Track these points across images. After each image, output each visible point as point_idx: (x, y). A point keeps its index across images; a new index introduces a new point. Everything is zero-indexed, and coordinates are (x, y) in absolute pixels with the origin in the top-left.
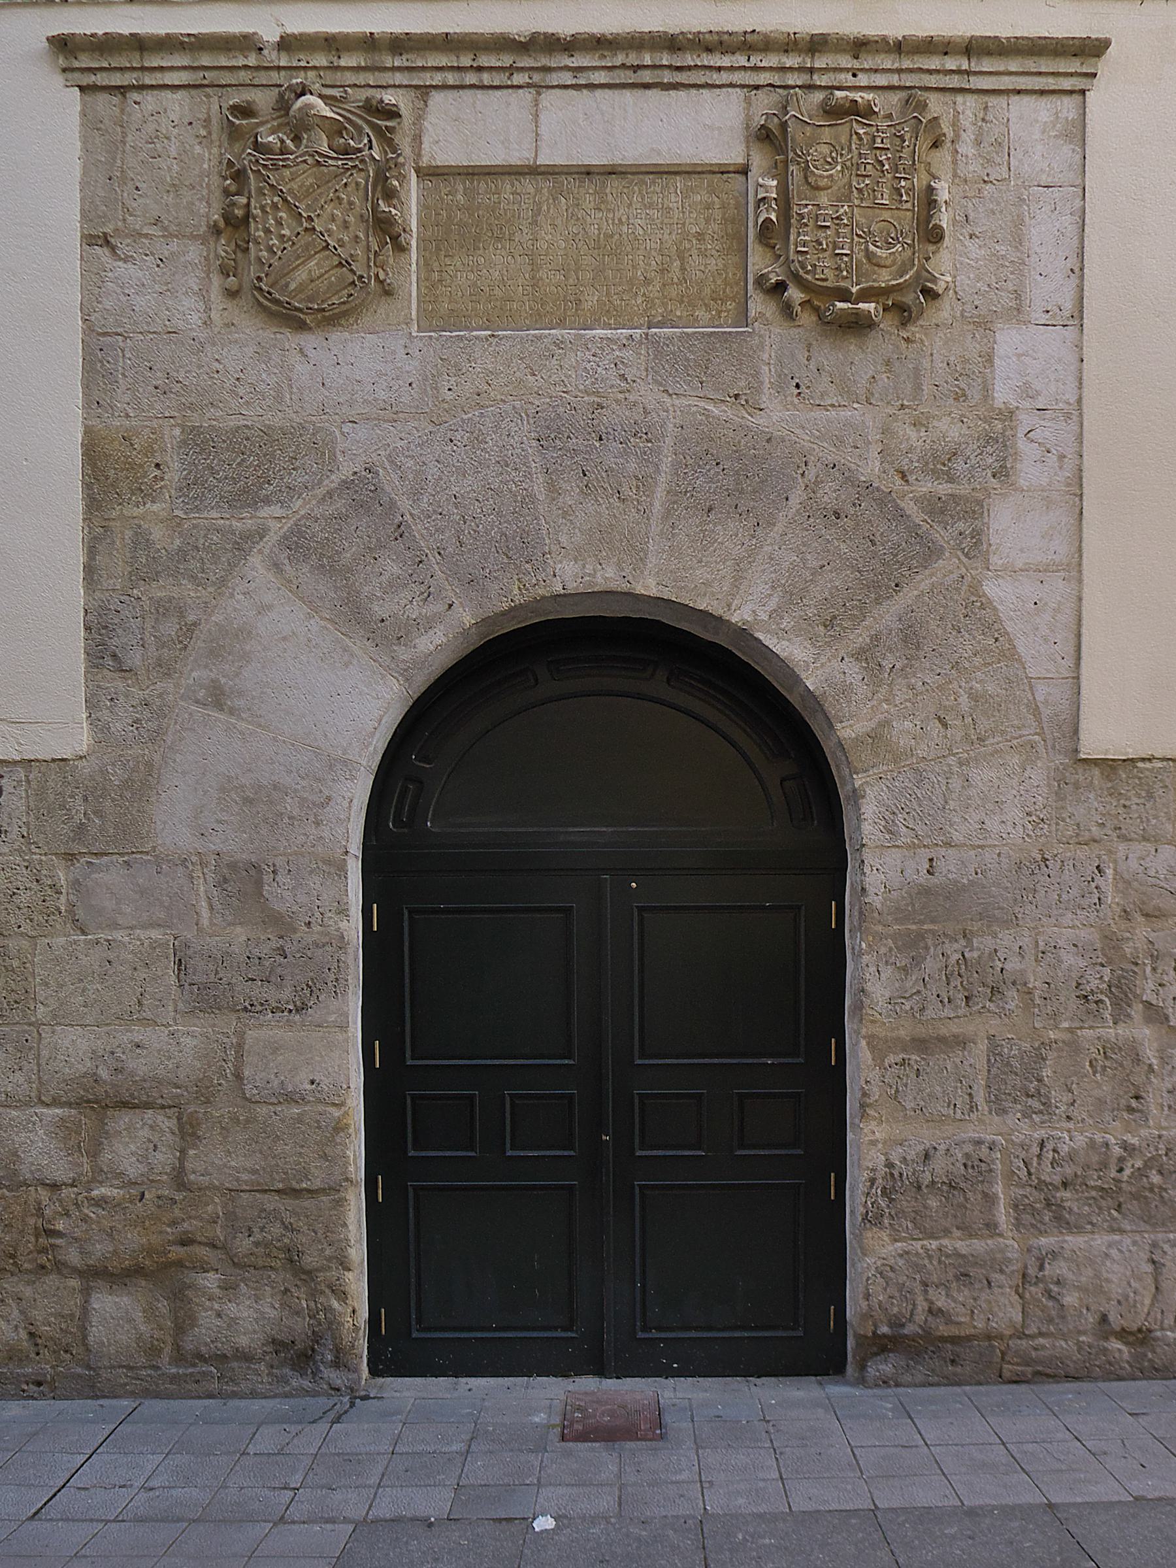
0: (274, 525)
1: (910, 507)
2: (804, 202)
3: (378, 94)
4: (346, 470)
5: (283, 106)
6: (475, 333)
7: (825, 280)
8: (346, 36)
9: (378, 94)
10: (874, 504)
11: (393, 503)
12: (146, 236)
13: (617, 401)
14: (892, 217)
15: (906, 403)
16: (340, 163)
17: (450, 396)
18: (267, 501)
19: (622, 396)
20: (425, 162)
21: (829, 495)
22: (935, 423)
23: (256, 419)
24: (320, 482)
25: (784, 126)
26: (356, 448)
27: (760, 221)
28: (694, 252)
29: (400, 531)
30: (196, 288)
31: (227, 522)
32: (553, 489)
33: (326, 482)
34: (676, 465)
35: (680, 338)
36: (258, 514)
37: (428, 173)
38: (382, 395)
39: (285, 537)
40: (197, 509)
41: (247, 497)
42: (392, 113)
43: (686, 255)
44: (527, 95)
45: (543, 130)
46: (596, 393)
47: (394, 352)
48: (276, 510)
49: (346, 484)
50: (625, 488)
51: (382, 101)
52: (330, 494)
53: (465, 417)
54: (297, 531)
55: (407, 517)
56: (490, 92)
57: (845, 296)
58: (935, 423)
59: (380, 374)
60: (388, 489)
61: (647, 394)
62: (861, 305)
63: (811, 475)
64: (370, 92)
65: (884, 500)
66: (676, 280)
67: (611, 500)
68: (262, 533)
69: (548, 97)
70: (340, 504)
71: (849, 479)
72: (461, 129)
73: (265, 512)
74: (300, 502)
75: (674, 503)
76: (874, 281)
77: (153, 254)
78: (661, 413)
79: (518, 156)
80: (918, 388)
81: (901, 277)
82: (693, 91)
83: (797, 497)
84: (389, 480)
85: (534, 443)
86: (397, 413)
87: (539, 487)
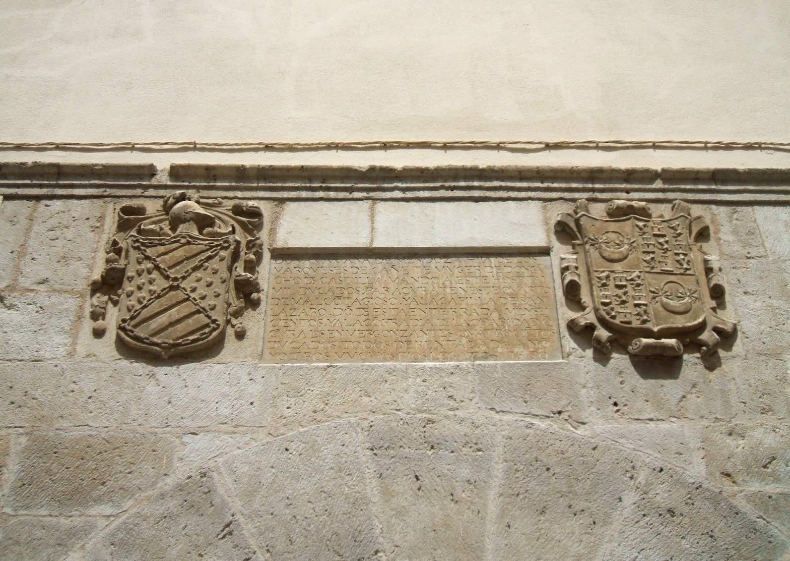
0: (102, 523)
1: (741, 504)
2: (602, 269)
3: (244, 203)
4: (180, 472)
5: (167, 208)
6: (314, 364)
7: (629, 323)
8: (330, 169)
9: (244, 203)
10: (707, 503)
11: (224, 504)
12: (32, 290)
13: (446, 417)
14: (678, 279)
15: (719, 416)
16: (207, 242)
17: (287, 413)
18: (98, 500)
19: (452, 413)
20: (279, 244)
21: (662, 495)
22: (751, 433)
23: (100, 429)
24: (154, 483)
25: (577, 221)
26: (195, 453)
27: (566, 281)
28: (510, 307)
29: (228, 530)
30: (67, 328)
31: (55, 520)
32: (387, 493)
33: (159, 485)
34: (507, 472)
35: (503, 366)
36: (87, 512)
37: (282, 254)
38: (226, 411)
39: (112, 535)
40: (28, 507)
41: (76, 496)
42: (256, 214)
43: (503, 309)
44: (366, 204)
45: (377, 225)
46: (428, 411)
47: (239, 379)
48: (108, 510)
49: (180, 488)
50: (459, 490)
51: (247, 205)
52: (162, 496)
53: (302, 430)
54: (126, 528)
55: (238, 517)
56: (335, 202)
57: (648, 334)
58: (751, 433)
59: (225, 395)
60: (221, 491)
61: (474, 410)
62: (663, 340)
63: (641, 477)
64: (237, 201)
65: (716, 499)
66: (495, 326)
67: (445, 502)
68: (87, 530)
69: (380, 206)
70: (172, 504)
71: (678, 482)
72: (302, 223)
73: (95, 510)
74: (131, 502)
75: (508, 503)
76: (672, 323)
77: (35, 304)
78: (490, 427)
79: (361, 241)
80: (726, 403)
81: (695, 320)
82: (500, 203)
83: (630, 498)
84: (223, 484)
85: (369, 453)
86: (236, 426)
87: (372, 488)
